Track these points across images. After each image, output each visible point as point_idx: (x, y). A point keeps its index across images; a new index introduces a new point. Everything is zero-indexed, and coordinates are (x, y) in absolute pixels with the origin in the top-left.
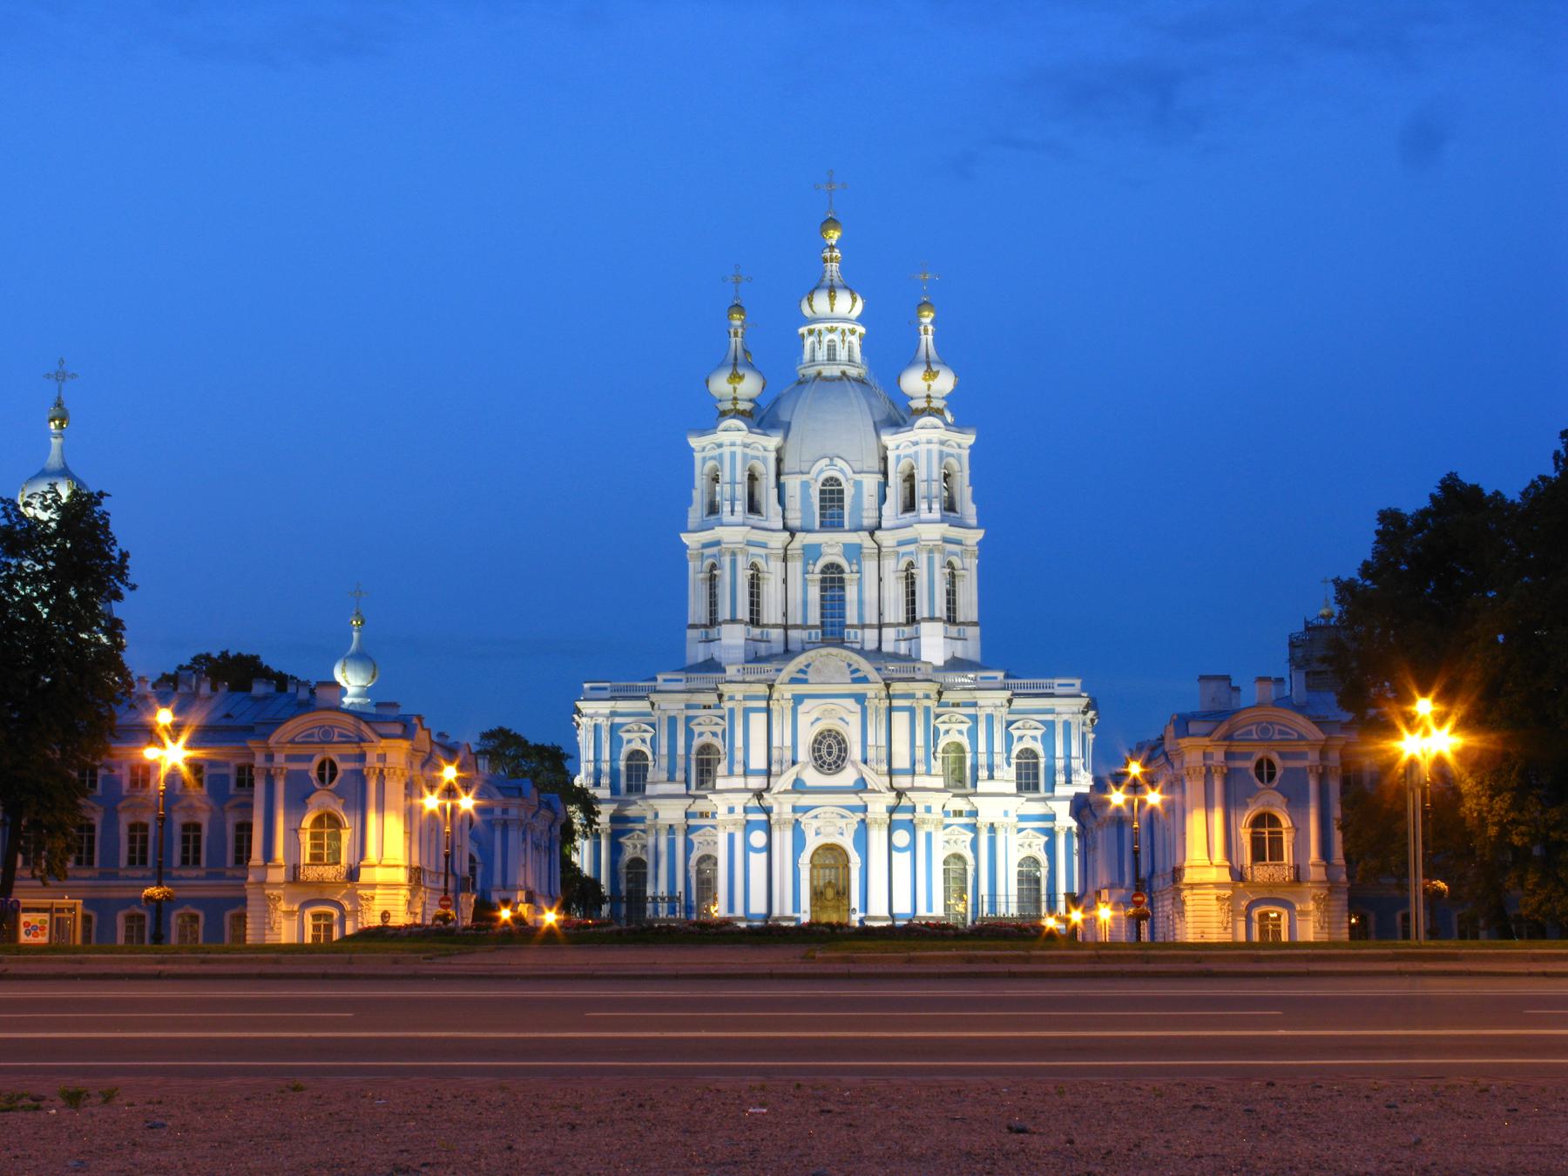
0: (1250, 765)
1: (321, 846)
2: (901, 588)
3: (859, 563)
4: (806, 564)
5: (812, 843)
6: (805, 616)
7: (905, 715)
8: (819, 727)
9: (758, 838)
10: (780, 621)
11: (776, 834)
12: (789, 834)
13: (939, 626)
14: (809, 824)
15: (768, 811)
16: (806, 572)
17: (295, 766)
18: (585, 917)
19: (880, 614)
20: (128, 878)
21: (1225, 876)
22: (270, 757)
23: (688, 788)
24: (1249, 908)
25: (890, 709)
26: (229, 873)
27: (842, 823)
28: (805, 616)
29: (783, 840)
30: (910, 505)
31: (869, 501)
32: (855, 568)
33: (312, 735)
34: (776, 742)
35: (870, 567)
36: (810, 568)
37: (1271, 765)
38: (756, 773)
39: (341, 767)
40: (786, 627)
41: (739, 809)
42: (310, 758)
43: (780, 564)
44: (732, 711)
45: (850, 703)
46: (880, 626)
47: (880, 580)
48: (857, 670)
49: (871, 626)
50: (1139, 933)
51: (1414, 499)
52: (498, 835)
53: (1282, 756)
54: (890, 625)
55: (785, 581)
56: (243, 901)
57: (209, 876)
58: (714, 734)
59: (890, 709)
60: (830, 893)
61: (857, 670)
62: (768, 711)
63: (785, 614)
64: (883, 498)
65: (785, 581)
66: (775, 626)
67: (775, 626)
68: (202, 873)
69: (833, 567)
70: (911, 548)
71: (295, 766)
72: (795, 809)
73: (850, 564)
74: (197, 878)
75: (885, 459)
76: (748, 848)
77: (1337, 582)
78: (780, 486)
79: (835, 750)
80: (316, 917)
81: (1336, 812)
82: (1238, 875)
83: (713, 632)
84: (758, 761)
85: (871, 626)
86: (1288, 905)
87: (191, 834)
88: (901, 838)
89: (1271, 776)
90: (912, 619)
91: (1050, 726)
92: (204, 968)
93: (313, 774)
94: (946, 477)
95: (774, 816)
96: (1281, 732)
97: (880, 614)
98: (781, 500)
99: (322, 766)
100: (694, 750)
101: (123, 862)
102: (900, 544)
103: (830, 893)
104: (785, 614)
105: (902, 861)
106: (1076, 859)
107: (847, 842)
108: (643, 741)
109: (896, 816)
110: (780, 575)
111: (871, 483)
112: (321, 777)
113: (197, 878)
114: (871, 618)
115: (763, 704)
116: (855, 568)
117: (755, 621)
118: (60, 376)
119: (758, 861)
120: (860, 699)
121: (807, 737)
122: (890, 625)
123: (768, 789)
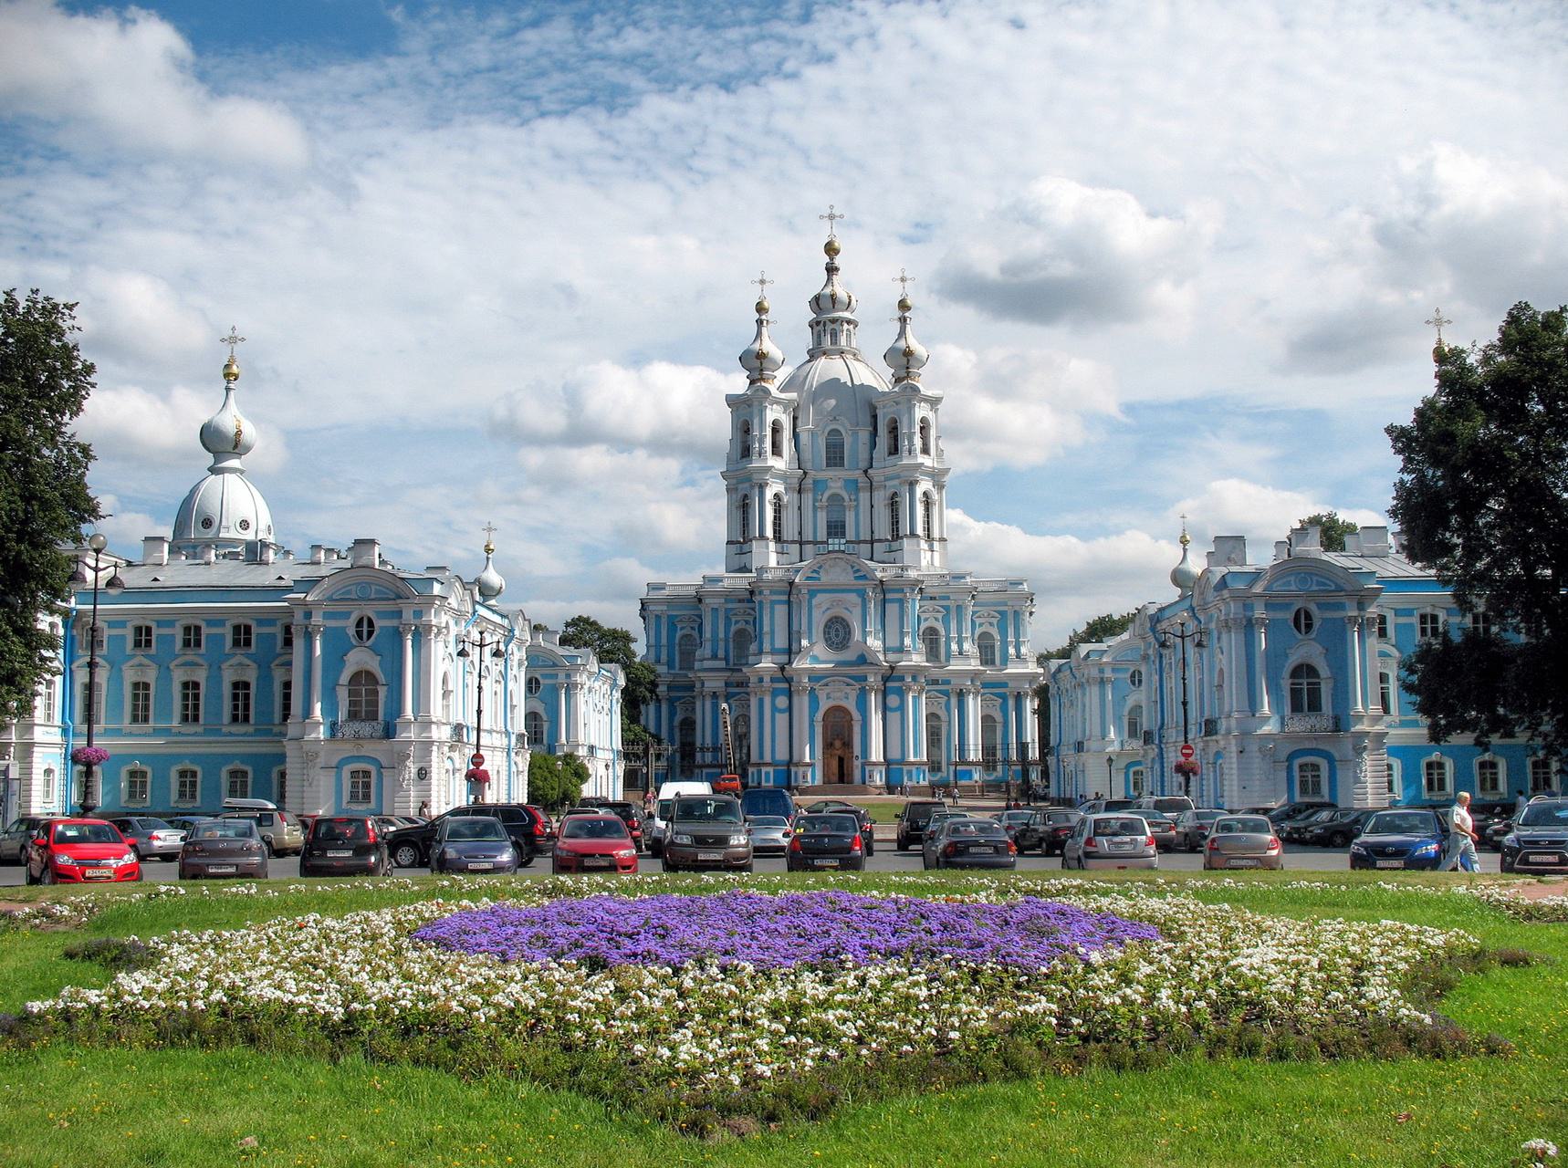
5: (824, 705)
6: (857, 534)
7: (896, 605)
8: (831, 703)
9: (782, 702)
11: (795, 699)
12: (806, 699)
14: (822, 695)
15: (789, 681)
16: (815, 500)
17: (332, 623)
18: (1476, 480)
20: (231, 734)
24: (1291, 757)
25: (884, 601)
26: (225, 730)
27: (848, 689)
28: (857, 534)
29: (802, 703)
33: (349, 592)
34: (795, 628)
35: (864, 497)
37: (1308, 616)
38: (892, 601)
39: (378, 624)
40: (801, 543)
41: (766, 679)
42: (347, 615)
44: (761, 602)
45: (853, 598)
49: (865, 542)
53: (1320, 606)
54: (880, 541)
56: (281, 758)
57: (206, 732)
59: (884, 601)
60: (838, 744)
62: (789, 603)
64: (873, 445)
66: (793, 542)
67: (793, 542)
68: (200, 729)
69: (836, 499)
70: (896, 482)
71: (332, 623)
74: (195, 734)
75: (875, 417)
76: (774, 709)
77: (1390, 430)
78: (795, 435)
79: (841, 634)
80: (354, 774)
83: (895, 545)
84: (781, 642)
85: (865, 542)
88: (893, 700)
89: (1309, 627)
91: (1003, 614)
93: (352, 631)
96: (1319, 583)
99: (360, 623)
101: (227, 717)
103: (838, 744)
105: (894, 717)
106: (819, 730)
107: (851, 705)
109: (889, 684)
111: (864, 436)
112: (359, 634)
113: (195, 734)
117: (929, 537)
119: (782, 719)
120: (862, 594)
121: (819, 619)
122: (880, 541)
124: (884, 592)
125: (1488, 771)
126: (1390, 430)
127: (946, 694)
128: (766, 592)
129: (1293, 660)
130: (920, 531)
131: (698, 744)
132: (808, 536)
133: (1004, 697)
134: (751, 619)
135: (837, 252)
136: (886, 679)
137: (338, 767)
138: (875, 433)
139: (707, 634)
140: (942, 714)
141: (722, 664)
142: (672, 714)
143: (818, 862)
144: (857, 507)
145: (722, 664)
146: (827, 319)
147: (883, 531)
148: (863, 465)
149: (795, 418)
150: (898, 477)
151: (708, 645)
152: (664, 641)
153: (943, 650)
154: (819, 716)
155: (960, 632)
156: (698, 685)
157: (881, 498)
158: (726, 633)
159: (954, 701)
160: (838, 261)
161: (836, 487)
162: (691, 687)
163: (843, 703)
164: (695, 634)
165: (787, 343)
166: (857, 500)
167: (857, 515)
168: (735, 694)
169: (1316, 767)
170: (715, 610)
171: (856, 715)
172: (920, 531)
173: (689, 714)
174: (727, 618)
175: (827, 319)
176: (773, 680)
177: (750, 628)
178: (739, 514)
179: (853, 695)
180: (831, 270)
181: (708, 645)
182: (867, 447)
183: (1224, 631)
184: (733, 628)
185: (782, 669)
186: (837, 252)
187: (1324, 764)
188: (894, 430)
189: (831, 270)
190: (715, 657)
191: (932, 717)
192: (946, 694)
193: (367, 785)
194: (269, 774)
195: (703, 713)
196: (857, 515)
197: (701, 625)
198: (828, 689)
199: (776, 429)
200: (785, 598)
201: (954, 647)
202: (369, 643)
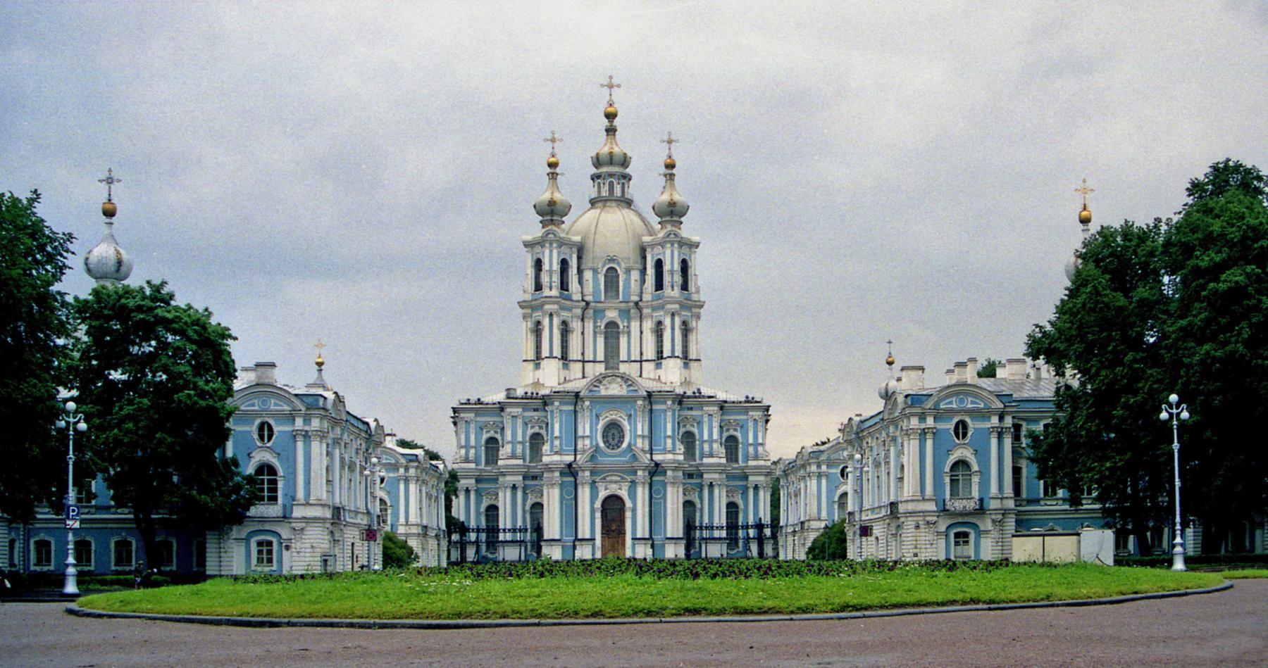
0: (951, 426)
1: (270, 490)
4: (595, 322)
5: (603, 494)
8: (608, 493)
10: (580, 358)
13: (678, 361)
16: (595, 327)
21: (931, 506)
24: (949, 527)
30: (659, 285)
31: (634, 286)
35: (635, 325)
39: (276, 429)
40: (584, 362)
43: (580, 323)
46: (641, 361)
50: (720, 539)
51: (1201, 172)
52: (402, 486)
55: (583, 333)
62: (575, 412)
63: (583, 354)
64: (643, 281)
65: (583, 333)
69: (612, 325)
75: (644, 258)
80: (260, 544)
81: (628, 514)
82: (944, 511)
86: (974, 526)
87: (265, 549)
90: (660, 355)
93: (256, 436)
98: (580, 282)
104: (583, 354)
106: (598, 515)
107: (624, 493)
109: (655, 479)
111: (635, 275)
112: (261, 437)
117: (564, 357)
124: (651, 403)
125: (265, 549)
129: (953, 458)
131: (697, 524)
132: (589, 356)
133: (701, 487)
136: (652, 474)
139: (509, 437)
140: (697, 501)
142: (478, 503)
144: (629, 333)
145: (520, 462)
146: (611, 172)
147: (650, 353)
149: (579, 258)
152: (473, 443)
154: (598, 504)
155: (711, 434)
157: (648, 325)
158: (524, 436)
159: (706, 492)
160: (617, 122)
161: (612, 315)
163: (619, 493)
165: (576, 186)
167: (629, 342)
169: (270, 543)
171: (628, 504)
173: (493, 502)
175: (611, 172)
176: (562, 474)
179: (625, 486)
180: (611, 131)
183: (906, 438)
187: (275, 540)
189: (611, 131)
190: (513, 456)
191: (688, 505)
193: (270, 552)
194: (108, 544)
195: (504, 501)
196: (629, 342)
197: (503, 429)
199: (564, 264)
200: (571, 408)
201: (706, 447)
202: (269, 445)
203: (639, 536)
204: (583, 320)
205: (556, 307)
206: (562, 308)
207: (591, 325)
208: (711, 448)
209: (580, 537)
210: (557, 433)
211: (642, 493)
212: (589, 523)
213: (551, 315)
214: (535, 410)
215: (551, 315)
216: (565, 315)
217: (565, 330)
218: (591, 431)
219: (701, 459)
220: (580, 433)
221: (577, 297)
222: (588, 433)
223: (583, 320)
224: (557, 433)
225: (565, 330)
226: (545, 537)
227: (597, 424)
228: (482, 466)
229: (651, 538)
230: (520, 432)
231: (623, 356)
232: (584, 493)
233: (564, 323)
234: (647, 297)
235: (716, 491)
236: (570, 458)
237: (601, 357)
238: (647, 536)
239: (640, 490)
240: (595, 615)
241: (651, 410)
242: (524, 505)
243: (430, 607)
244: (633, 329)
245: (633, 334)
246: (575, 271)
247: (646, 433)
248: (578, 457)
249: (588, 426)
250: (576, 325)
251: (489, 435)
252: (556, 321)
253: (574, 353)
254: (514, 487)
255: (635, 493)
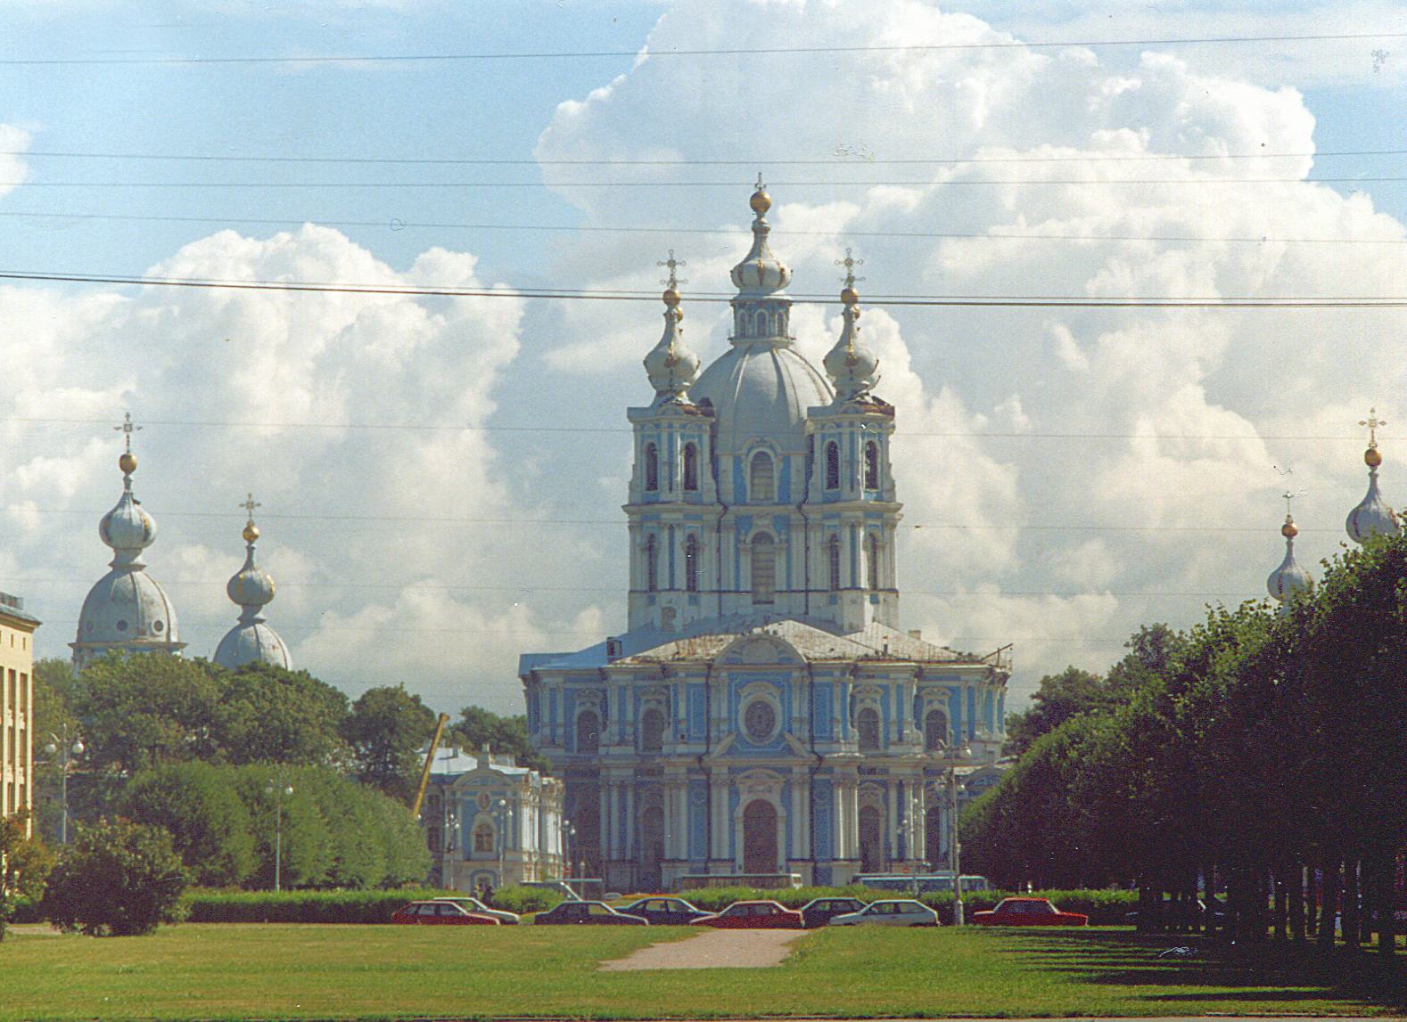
2: (826, 559)
3: (788, 534)
5: (745, 799)
6: (737, 585)
8: (754, 797)
12: (725, 793)
16: (738, 541)
17: (468, 798)
19: (807, 580)
22: (454, 793)
23: (637, 748)
32: (783, 537)
35: (797, 539)
36: (742, 538)
42: (475, 794)
43: (714, 535)
44: (675, 685)
46: (807, 591)
47: (807, 549)
48: (783, 652)
55: (719, 550)
58: (659, 702)
61: (783, 652)
64: (809, 474)
65: (719, 550)
69: (761, 538)
70: (835, 522)
72: (731, 770)
73: (780, 534)
77: (1070, 667)
78: (714, 460)
81: (781, 827)
92: (1097, 960)
94: (782, 945)
95: (713, 778)
97: (807, 580)
98: (715, 475)
100: (641, 716)
102: (826, 517)
104: (719, 580)
106: (740, 827)
107: (775, 799)
108: (659, 702)
110: (714, 543)
114: (798, 583)
115: (702, 680)
116: (783, 537)
117: (692, 586)
118: (250, 505)
123: (708, 753)
124: (811, 674)
126: (1070, 667)
127: (885, 785)
128: (682, 674)
130: (864, 583)
134: (663, 698)
135: (766, 206)
137: (472, 876)
138: (810, 460)
140: (880, 806)
141: (630, 750)
143: (722, 228)
144: (788, 550)
147: (820, 579)
148: (796, 497)
149: (713, 437)
150: (838, 516)
151: (614, 729)
152: (560, 719)
153: (881, 736)
154: (740, 812)
156: (603, 773)
157: (817, 538)
158: (636, 711)
159: (893, 795)
162: (595, 773)
163: (766, 797)
164: (597, 711)
166: (788, 541)
167: (789, 562)
168: (642, 784)
170: (623, 689)
171: (781, 811)
172: (864, 583)
174: (637, 699)
177: (663, 709)
178: (645, 557)
179: (777, 788)
181: (614, 729)
182: (803, 477)
184: (642, 710)
185: (700, 759)
186: (766, 206)
188: (832, 453)
190: (622, 742)
192: (885, 785)
196: (789, 562)
198: (749, 782)
203: (796, 855)
204: (719, 530)
205: (680, 516)
206: (687, 517)
207: (732, 537)
208: (900, 733)
209: (714, 856)
210: (682, 714)
211: (800, 797)
212: (729, 839)
213: (671, 528)
214: (653, 678)
215: (671, 528)
216: (693, 526)
217: (693, 549)
218: (730, 712)
219: (886, 747)
220: (714, 714)
221: (710, 497)
222: (724, 714)
223: (719, 530)
224: (682, 714)
225: (693, 549)
226: (667, 856)
227: (738, 702)
228: (575, 753)
229: (812, 859)
230: (630, 708)
231: (781, 584)
232: (721, 797)
233: (691, 537)
234: (814, 496)
235: (909, 793)
236: (701, 749)
237: (746, 585)
238: (807, 856)
239: (796, 794)
240: (768, 1014)
241: (812, 685)
242: (636, 808)
243: (968, 815)
244: (794, 543)
245: (794, 551)
246: (707, 455)
247: (806, 715)
248: (712, 747)
249: (724, 706)
250: (708, 539)
251: (583, 708)
252: (680, 537)
253: (706, 578)
254: (622, 787)
255: (790, 796)
